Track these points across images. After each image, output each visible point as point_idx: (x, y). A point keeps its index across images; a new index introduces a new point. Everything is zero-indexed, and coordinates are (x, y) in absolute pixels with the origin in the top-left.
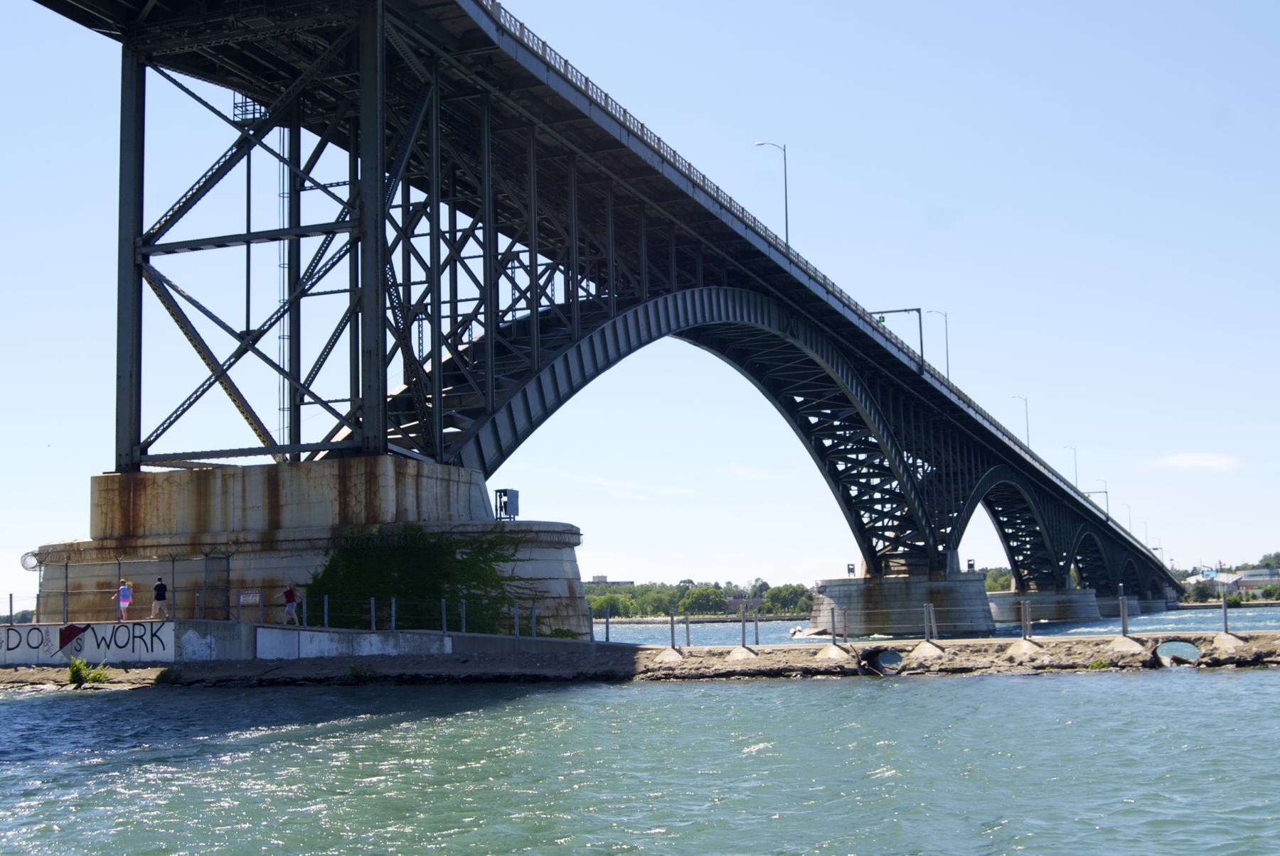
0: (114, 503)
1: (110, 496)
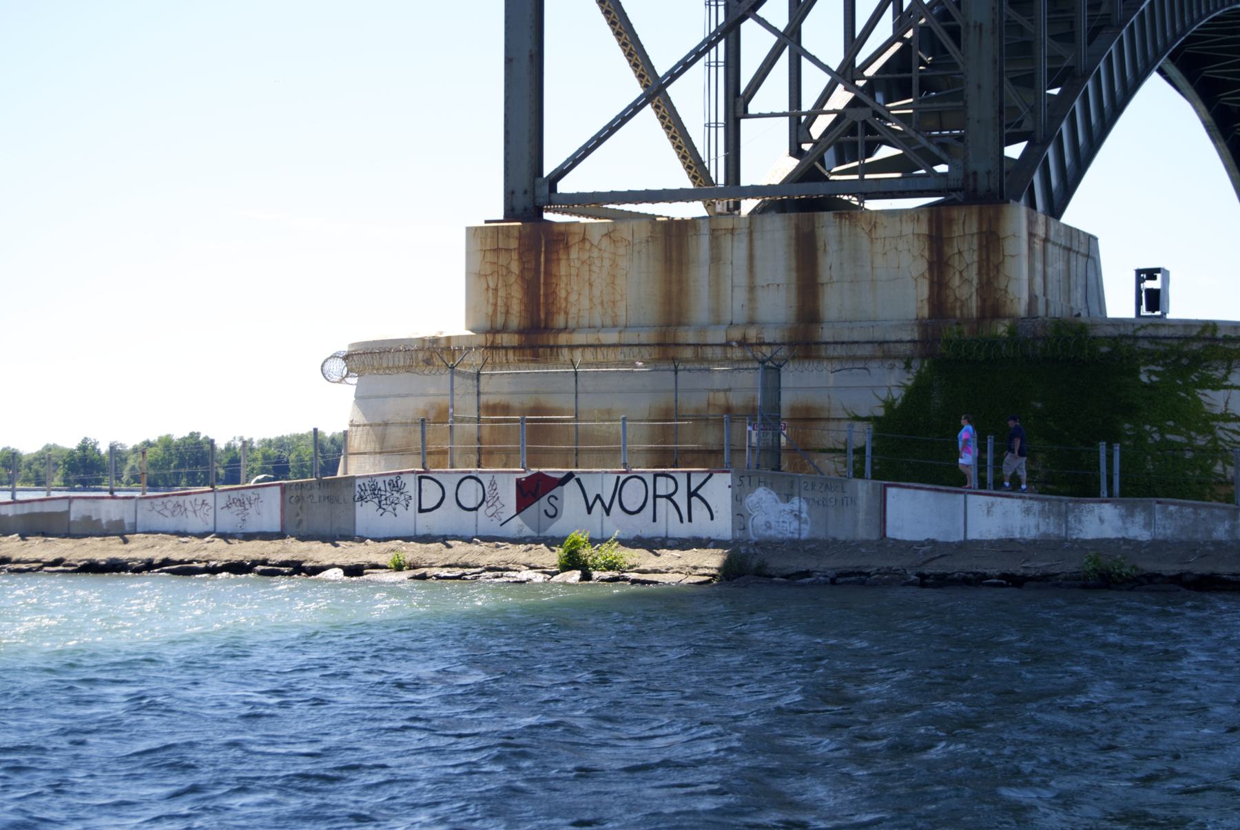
0: (509, 272)
1: (503, 259)
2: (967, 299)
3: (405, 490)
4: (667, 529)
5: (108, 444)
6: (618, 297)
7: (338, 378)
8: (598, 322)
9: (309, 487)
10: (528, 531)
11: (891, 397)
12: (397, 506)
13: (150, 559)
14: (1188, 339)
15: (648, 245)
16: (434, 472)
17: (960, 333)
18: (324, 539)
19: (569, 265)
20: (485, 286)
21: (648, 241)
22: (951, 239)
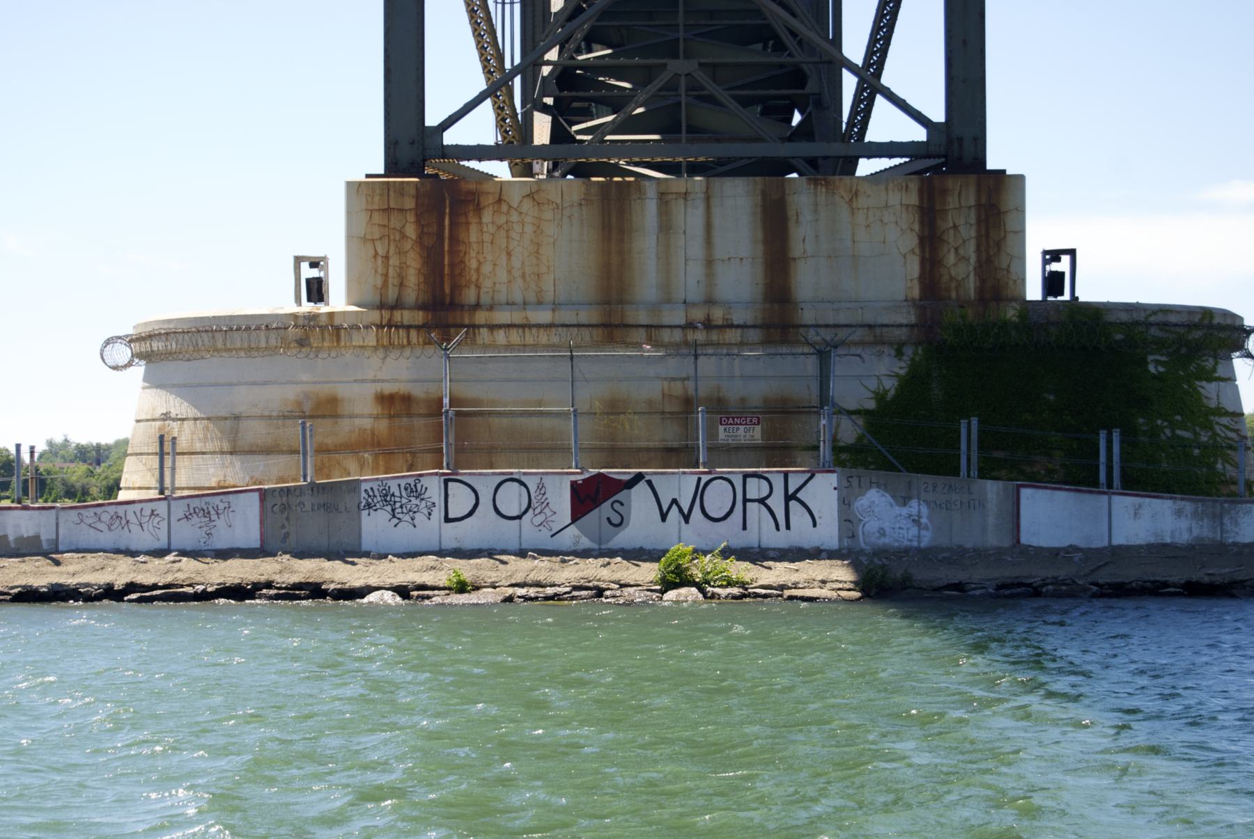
0: (404, 236)
1: (395, 221)
2: (963, 279)
3: (426, 496)
4: (760, 538)
5: (45, 441)
6: (544, 269)
7: (110, 362)
8: (518, 298)
9: (298, 493)
10: (586, 543)
11: (881, 387)
12: (416, 515)
13: (108, 584)
14: (1191, 326)
15: (581, 209)
16: (465, 474)
17: (962, 317)
18: (330, 556)
19: (481, 230)
20: (372, 252)
21: (581, 205)
22: (945, 211)
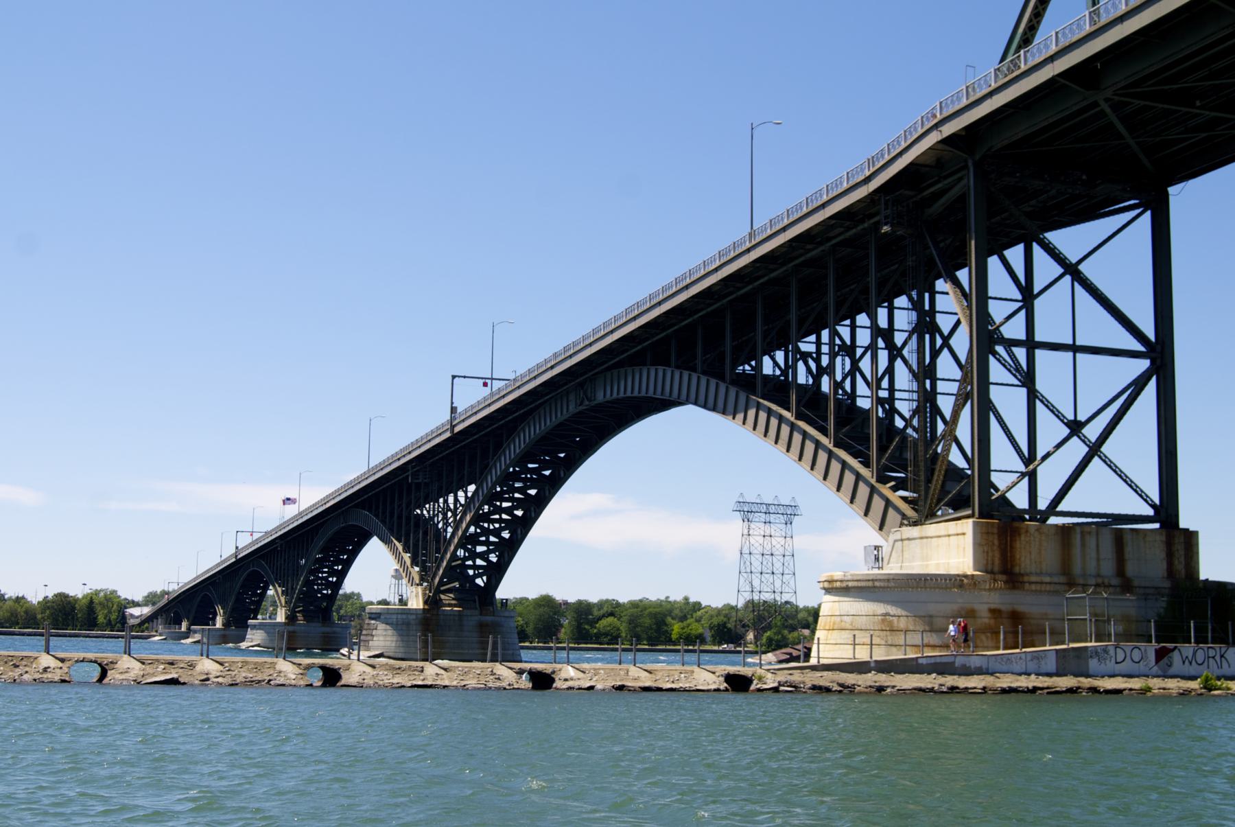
0: (993, 544)
10: (1160, 673)
